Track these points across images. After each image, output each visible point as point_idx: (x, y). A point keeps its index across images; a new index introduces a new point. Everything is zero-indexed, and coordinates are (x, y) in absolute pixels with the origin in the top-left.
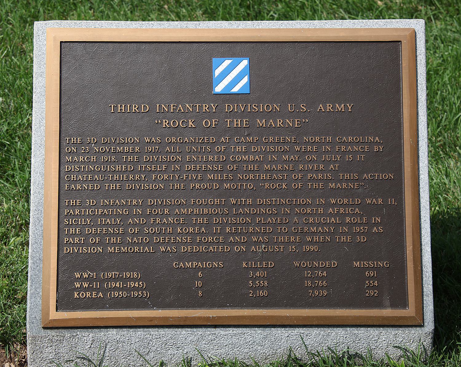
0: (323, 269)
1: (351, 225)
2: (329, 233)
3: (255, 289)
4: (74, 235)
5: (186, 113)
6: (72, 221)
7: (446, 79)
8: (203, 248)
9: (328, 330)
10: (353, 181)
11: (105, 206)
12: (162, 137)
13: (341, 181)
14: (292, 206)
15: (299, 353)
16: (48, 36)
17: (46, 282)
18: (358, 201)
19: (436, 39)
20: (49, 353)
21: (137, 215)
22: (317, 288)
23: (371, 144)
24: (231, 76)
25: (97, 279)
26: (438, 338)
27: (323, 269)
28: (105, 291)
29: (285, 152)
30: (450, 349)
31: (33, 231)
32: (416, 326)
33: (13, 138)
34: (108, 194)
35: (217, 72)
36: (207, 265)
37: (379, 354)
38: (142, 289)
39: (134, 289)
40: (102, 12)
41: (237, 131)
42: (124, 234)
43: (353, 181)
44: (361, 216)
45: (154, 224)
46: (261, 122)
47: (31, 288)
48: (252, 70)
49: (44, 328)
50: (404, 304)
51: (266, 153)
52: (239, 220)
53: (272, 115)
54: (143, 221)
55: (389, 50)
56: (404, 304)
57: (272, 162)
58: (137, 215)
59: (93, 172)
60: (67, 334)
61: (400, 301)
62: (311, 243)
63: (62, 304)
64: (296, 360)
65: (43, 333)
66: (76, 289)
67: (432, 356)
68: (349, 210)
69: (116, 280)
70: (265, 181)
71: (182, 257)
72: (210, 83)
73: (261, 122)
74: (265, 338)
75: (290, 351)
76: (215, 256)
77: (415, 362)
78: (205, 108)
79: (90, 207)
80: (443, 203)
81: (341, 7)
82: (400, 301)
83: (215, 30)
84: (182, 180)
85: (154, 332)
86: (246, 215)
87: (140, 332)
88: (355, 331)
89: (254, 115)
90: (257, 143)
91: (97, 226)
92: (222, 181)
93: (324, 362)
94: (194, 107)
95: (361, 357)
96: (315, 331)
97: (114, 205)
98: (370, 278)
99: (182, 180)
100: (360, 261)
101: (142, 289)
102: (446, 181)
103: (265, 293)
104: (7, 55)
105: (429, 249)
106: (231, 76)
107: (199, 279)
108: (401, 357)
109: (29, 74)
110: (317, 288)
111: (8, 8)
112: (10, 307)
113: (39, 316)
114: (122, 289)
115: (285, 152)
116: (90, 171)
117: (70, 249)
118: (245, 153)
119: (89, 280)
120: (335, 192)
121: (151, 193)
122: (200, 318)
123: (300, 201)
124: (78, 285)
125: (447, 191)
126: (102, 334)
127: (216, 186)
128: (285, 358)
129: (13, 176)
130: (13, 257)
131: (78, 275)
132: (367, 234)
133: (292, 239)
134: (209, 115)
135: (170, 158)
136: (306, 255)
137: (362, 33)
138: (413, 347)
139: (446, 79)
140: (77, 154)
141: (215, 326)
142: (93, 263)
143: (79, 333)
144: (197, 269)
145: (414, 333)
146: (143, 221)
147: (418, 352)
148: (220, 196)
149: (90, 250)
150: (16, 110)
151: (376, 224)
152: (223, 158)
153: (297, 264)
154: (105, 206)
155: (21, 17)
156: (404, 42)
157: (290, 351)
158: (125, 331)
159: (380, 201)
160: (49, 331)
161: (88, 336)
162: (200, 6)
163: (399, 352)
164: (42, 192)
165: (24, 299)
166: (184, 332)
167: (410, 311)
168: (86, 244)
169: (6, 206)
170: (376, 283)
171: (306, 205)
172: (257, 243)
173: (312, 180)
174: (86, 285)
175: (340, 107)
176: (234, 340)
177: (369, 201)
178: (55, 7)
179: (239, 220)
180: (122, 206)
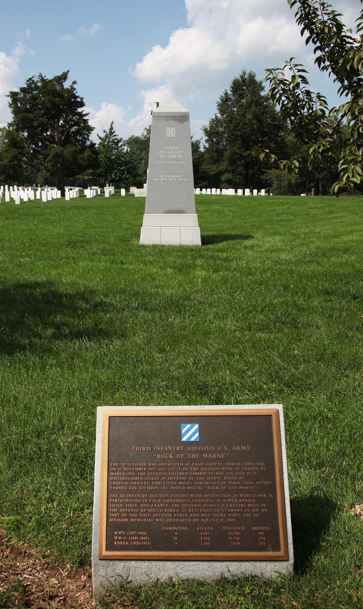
0: (238, 531)
1: (251, 508)
2: (240, 512)
3: (204, 541)
4: (114, 513)
5: (168, 451)
6: (113, 505)
7: (298, 426)
8: (177, 520)
9: (241, 563)
10: (251, 485)
11: (129, 498)
12: (157, 463)
13: (245, 485)
14: (221, 498)
15: (227, 575)
16: (104, 413)
17: (101, 536)
18: (254, 496)
19: (292, 405)
20: (102, 572)
21: (145, 503)
22: (235, 541)
23: (260, 466)
24: (190, 433)
25: (126, 535)
26: (296, 566)
27: (238, 531)
28: (129, 542)
29: (217, 471)
30: (302, 572)
31: (95, 509)
32: (285, 561)
33: (87, 458)
34: (131, 492)
35: (184, 431)
36: (180, 528)
37: (267, 575)
38: (147, 541)
39: (144, 540)
40: (131, 392)
41: (194, 460)
42: (139, 512)
43: (251, 485)
44: (256, 503)
45: (153, 507)
46: (205, 456)
47: (94, 539)
48: (200, 430)
49: (100, 559)
50: (279, 549)
51: (208, 471)
52: (195, 505)
53: (211, 452)
54: (148, 505)
55: (266, 420)
56: (279, 549)
57: (211, 476)
58: (145, 503)
59: (124, 481)
60: (111, 563)
61: (276, 548)
62: (231, 517)
63: (109, 547)
64: (225, 578)
65: (100, 562)
66: (115, 540)
67: (294, 576)
68: (250, 500)
69: (134, 536)
70: (208, 485)
71: (167, 525)
72: (180, 436)
73: (205, 456)
74: (209, 567)
75: (222, 574)
76: (184, 524)
77: (285, 579)
78: (178, 449)
79: (122, 498)
80: (298, 492)
81: (246, 389)
82: (276, 548)
83: (182, 410)
84: (167, 485)
85: (154, 563)
86: (199, 503)
87: (147, 563)
88: (255, 563)
89: (201, 452)
90: (203, 466)
91: (125, 508)
92: (186, 486)
93: (239, 580)
94: (172, 448)
95: (258, 577)
96: (234, 563)
97: (134, 498)
98: (261, 536)
99: (167, 485)
100: (256, 526)
101: (147, 541)
102: (300, 480)
103: (208, 543)
104: (85, 415)
105: (290, 522)
106: (190, 433)
107: (175, 536)
108: (278, 577)
109: (94, 425)
110: (235, 541)
111: (87, 391)
112: (84, 546)
113: (97, 553)
114: (138, 541)
115: (217, 471)
116: (122, 480)
117: (112, 520)
118: (197, 471)
119: (122, 535)
120: (242, 491)
121: (152, 491)
122: (176, 556)
123: (225, 496)
124: (116, 538)
125: (300, 485)
126: (128, 564)
127: (183, 488)
128: (219, 577)
129: (87, 477)
130: (86, 520)
131: (116, 533)
132: (259, 512)
133: (222, 515)
134: (180, 452)
135: (161, 473)
136: (229, 524)
137: (253, 411)
138: (284, 572)
139: (298, 426)
140: (116, 471)
141: (184, 561)
142: (124, 527)
143: (117, 563)
144: (175, 531)
145: (284, 564)
146: (148, 505)
147: (286, 574)
148: (185, 493)
149: (122, 520)
150: (89, 443)
151: (263, 508)
152: (187, 473)
153: (224, 528)
154: (129, 498)
155: (93, 396)
156: (273, 415)
157: (222, 574)
158: (139, 563)
159: (265, 496)
160: (102, 561)
161: (121, 564)
162: (178, 389)
163: (277, 575)
164: (99, 490)
165: (90, 542)
166: (168, 564)
167: (281, 553)
168: (120, 517)
169: (83, 493)
170: (264, 538)
171: (229, 498)
172: (205, 517)
173: (231, 485)
174: (120, 538)
175: (244, 448)
176: (194, 568)
177: (259, 496)
178: (108, 390)
179: (195, 505)
180: (138, 498)
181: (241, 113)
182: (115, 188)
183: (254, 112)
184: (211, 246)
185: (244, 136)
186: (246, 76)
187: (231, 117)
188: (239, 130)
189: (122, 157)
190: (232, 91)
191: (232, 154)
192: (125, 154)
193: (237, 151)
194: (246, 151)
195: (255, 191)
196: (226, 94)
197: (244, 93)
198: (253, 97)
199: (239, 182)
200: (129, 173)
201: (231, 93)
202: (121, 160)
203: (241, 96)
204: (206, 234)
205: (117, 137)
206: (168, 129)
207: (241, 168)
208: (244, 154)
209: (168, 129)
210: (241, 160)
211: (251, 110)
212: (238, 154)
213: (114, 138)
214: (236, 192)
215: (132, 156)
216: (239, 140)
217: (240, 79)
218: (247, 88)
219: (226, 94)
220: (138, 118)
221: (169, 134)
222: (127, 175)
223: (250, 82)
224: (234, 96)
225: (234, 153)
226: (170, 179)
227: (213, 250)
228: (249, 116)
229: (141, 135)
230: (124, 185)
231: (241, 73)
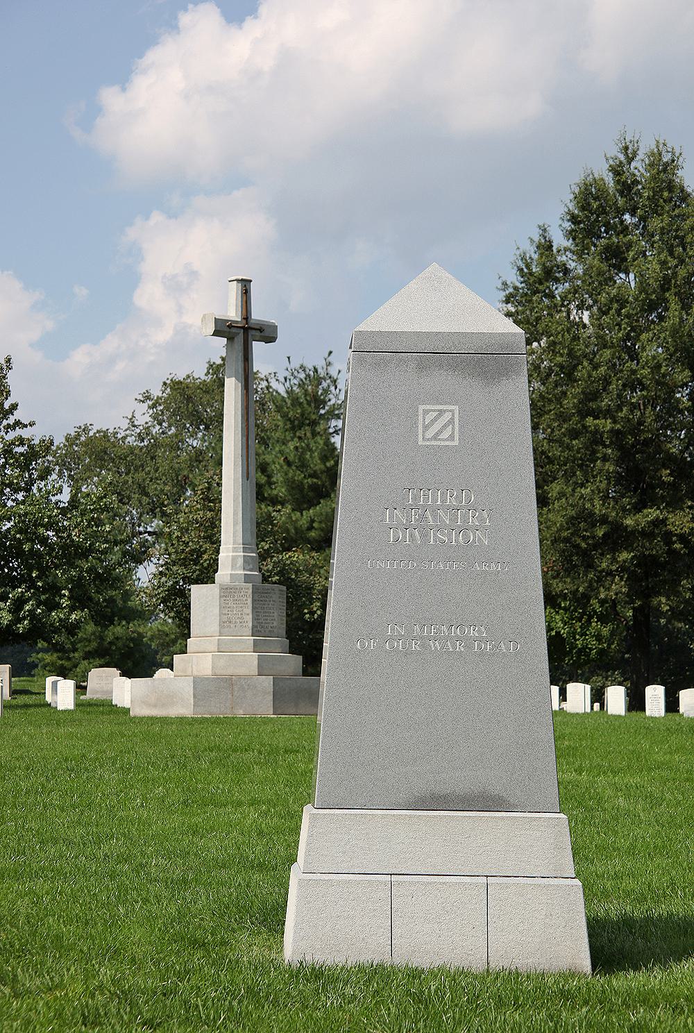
181: (615, 336)
182: (13, 674)
183: (675, 332)
184: (652, 979)
185: (630, 440)
186: (639, 167)
187: (571, 354)
188: (608, 413)
189: (48, 527)
190: (571, 234)
191: (572, 521)
192: (64, 511)
193: (598, 507)
194: (638, 508)
195: (655, 695)
196: (546, 247)
197: (629, 246)
198: (672, 262)
199: (602, 652)
200: (80, 600)
201: (569, 244)
202: (44, 541)
203: (617, 258)
204: (613, 909)
205: (25, 433)
206: (426, 412)
207: (618, 587)
208: (629, 522)
209: (426, 412)
210: (615, 549)
211: (661, 318)
212: (604, 520)
213: (11, 436)
214: (598, 696)
215: (99, 523)
216: (605, 459)
217: (609, 180)
218: (643, 219)
219: (546, 247)
220: (111, 344)
221: (431, 433)
222: (72, 609)
223: (657, 193)
224: (580, 255)
225: (585, 517)
226: (435, 646)
227: (647, 999)
228: (653, 351)
229: (125, 424)
230: (48, 658)
231: (615, 153)
